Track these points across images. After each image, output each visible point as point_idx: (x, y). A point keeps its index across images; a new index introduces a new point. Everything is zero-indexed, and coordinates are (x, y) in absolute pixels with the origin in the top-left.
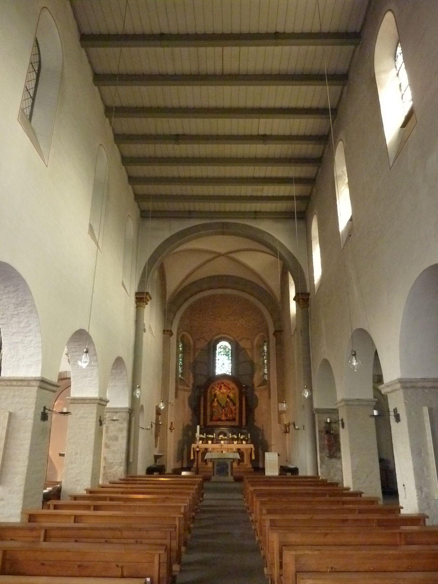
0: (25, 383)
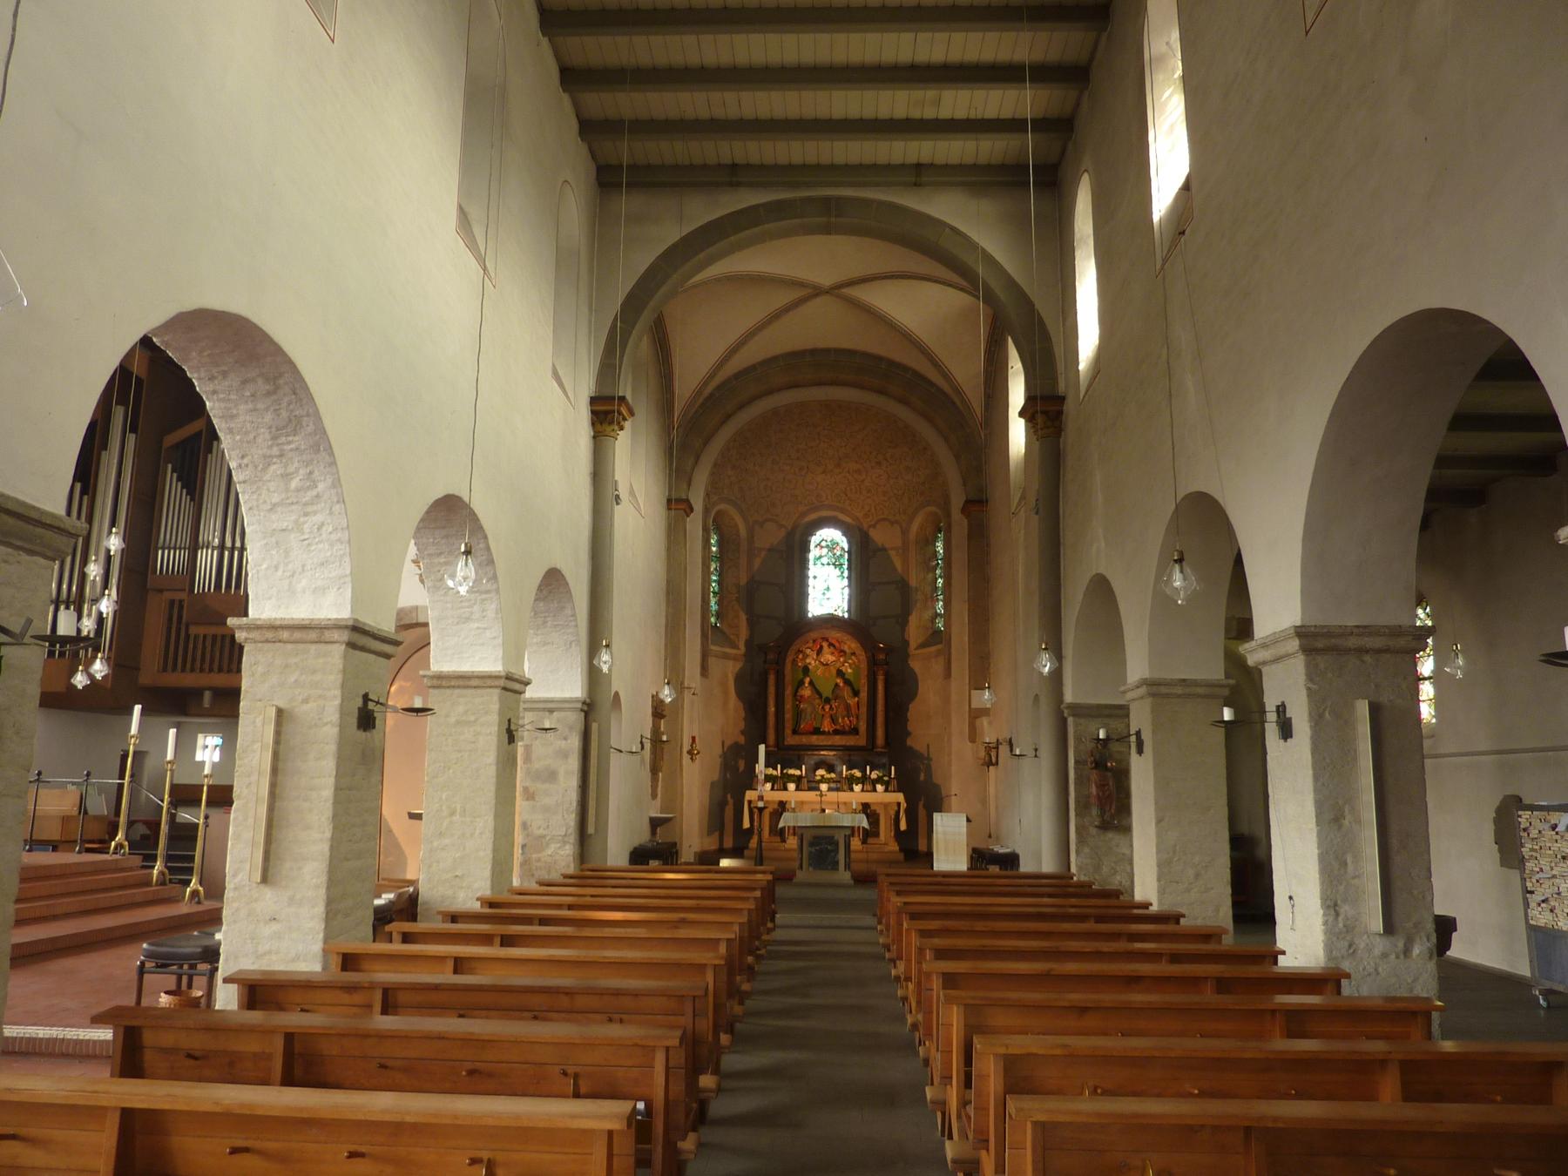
0: (313, 635)
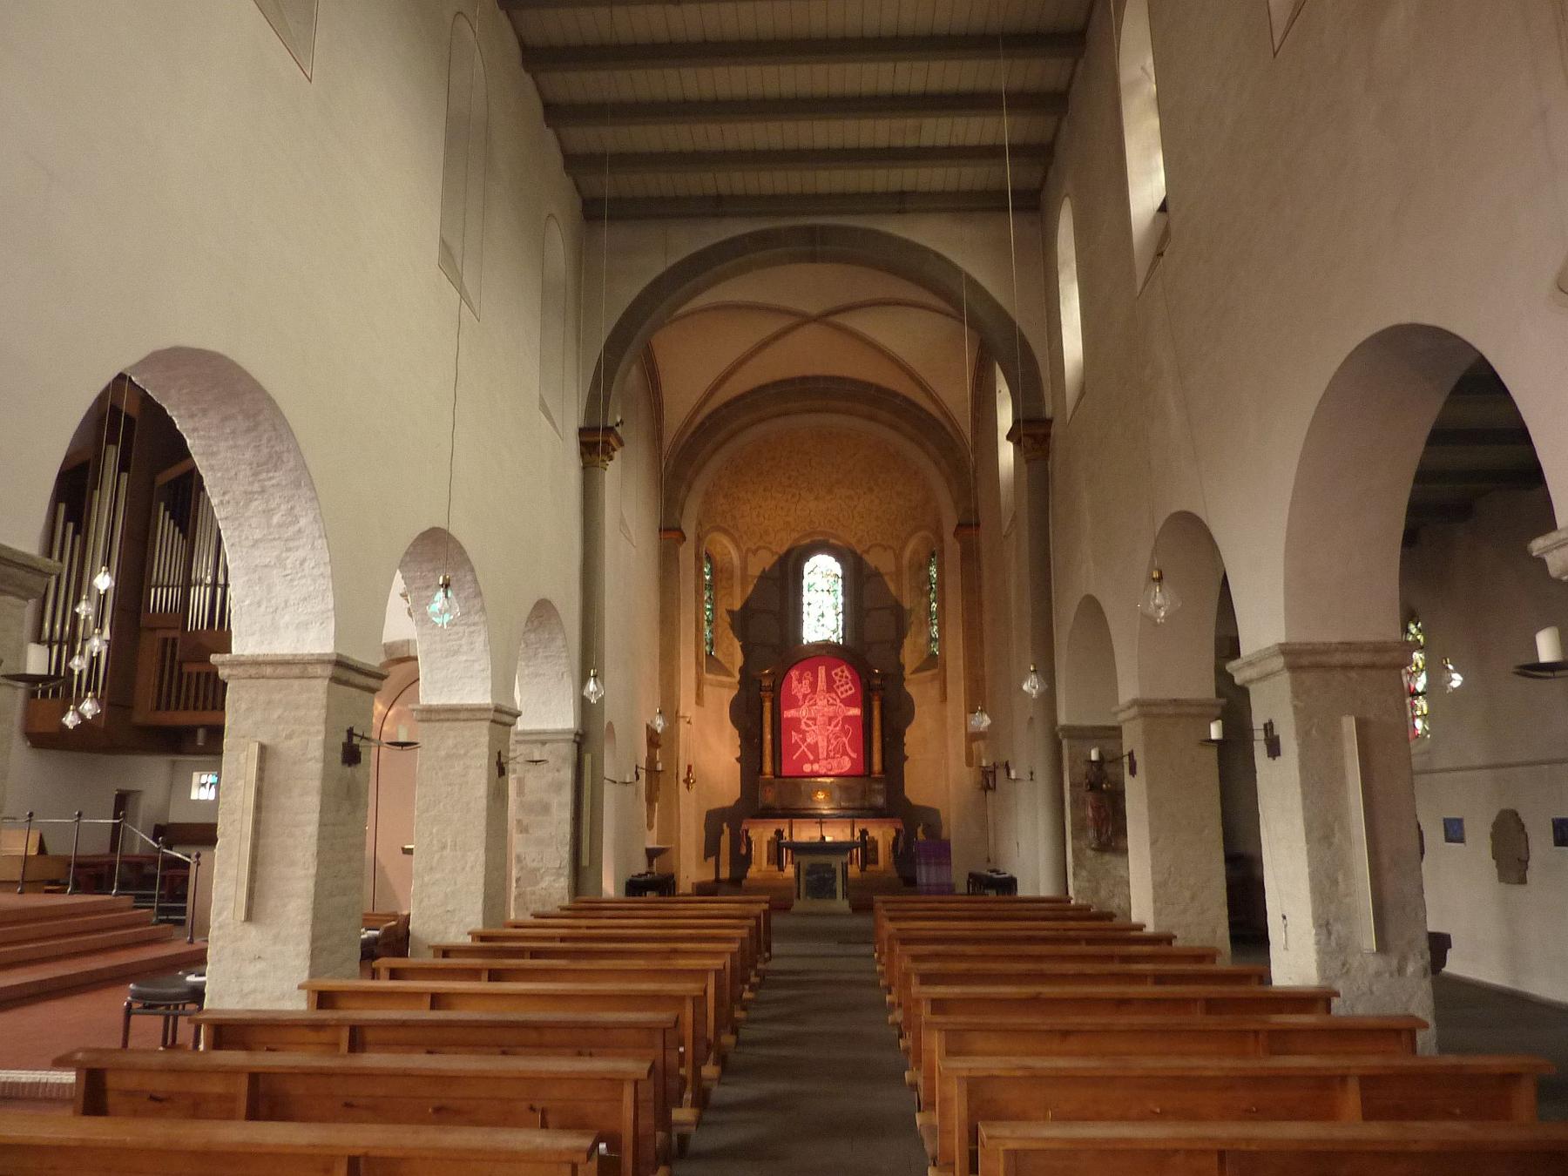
0: (296, 670)
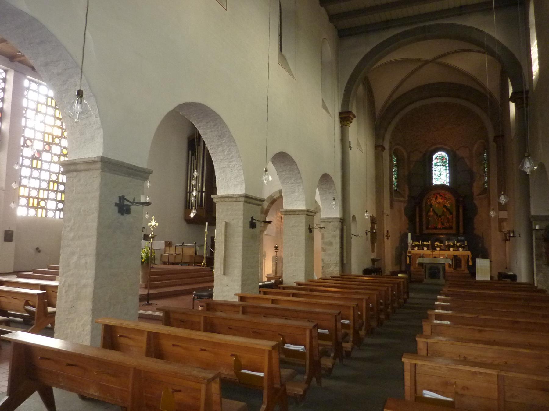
0: (234, 199)
